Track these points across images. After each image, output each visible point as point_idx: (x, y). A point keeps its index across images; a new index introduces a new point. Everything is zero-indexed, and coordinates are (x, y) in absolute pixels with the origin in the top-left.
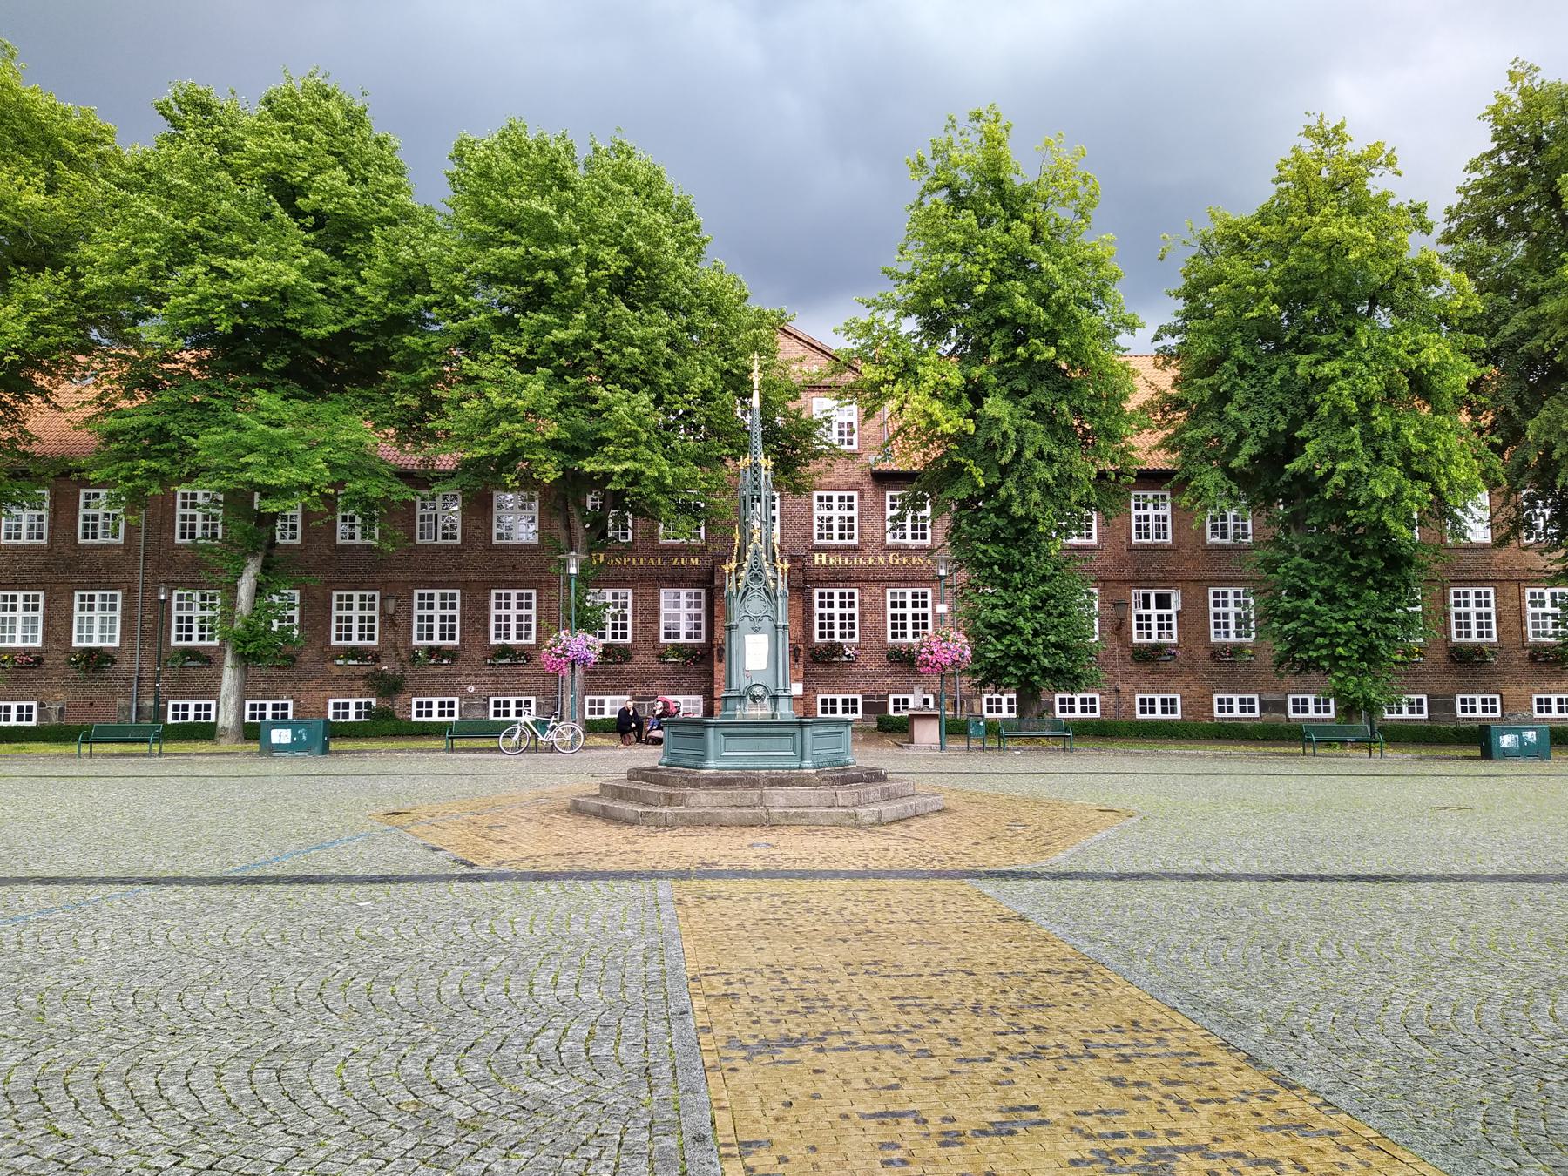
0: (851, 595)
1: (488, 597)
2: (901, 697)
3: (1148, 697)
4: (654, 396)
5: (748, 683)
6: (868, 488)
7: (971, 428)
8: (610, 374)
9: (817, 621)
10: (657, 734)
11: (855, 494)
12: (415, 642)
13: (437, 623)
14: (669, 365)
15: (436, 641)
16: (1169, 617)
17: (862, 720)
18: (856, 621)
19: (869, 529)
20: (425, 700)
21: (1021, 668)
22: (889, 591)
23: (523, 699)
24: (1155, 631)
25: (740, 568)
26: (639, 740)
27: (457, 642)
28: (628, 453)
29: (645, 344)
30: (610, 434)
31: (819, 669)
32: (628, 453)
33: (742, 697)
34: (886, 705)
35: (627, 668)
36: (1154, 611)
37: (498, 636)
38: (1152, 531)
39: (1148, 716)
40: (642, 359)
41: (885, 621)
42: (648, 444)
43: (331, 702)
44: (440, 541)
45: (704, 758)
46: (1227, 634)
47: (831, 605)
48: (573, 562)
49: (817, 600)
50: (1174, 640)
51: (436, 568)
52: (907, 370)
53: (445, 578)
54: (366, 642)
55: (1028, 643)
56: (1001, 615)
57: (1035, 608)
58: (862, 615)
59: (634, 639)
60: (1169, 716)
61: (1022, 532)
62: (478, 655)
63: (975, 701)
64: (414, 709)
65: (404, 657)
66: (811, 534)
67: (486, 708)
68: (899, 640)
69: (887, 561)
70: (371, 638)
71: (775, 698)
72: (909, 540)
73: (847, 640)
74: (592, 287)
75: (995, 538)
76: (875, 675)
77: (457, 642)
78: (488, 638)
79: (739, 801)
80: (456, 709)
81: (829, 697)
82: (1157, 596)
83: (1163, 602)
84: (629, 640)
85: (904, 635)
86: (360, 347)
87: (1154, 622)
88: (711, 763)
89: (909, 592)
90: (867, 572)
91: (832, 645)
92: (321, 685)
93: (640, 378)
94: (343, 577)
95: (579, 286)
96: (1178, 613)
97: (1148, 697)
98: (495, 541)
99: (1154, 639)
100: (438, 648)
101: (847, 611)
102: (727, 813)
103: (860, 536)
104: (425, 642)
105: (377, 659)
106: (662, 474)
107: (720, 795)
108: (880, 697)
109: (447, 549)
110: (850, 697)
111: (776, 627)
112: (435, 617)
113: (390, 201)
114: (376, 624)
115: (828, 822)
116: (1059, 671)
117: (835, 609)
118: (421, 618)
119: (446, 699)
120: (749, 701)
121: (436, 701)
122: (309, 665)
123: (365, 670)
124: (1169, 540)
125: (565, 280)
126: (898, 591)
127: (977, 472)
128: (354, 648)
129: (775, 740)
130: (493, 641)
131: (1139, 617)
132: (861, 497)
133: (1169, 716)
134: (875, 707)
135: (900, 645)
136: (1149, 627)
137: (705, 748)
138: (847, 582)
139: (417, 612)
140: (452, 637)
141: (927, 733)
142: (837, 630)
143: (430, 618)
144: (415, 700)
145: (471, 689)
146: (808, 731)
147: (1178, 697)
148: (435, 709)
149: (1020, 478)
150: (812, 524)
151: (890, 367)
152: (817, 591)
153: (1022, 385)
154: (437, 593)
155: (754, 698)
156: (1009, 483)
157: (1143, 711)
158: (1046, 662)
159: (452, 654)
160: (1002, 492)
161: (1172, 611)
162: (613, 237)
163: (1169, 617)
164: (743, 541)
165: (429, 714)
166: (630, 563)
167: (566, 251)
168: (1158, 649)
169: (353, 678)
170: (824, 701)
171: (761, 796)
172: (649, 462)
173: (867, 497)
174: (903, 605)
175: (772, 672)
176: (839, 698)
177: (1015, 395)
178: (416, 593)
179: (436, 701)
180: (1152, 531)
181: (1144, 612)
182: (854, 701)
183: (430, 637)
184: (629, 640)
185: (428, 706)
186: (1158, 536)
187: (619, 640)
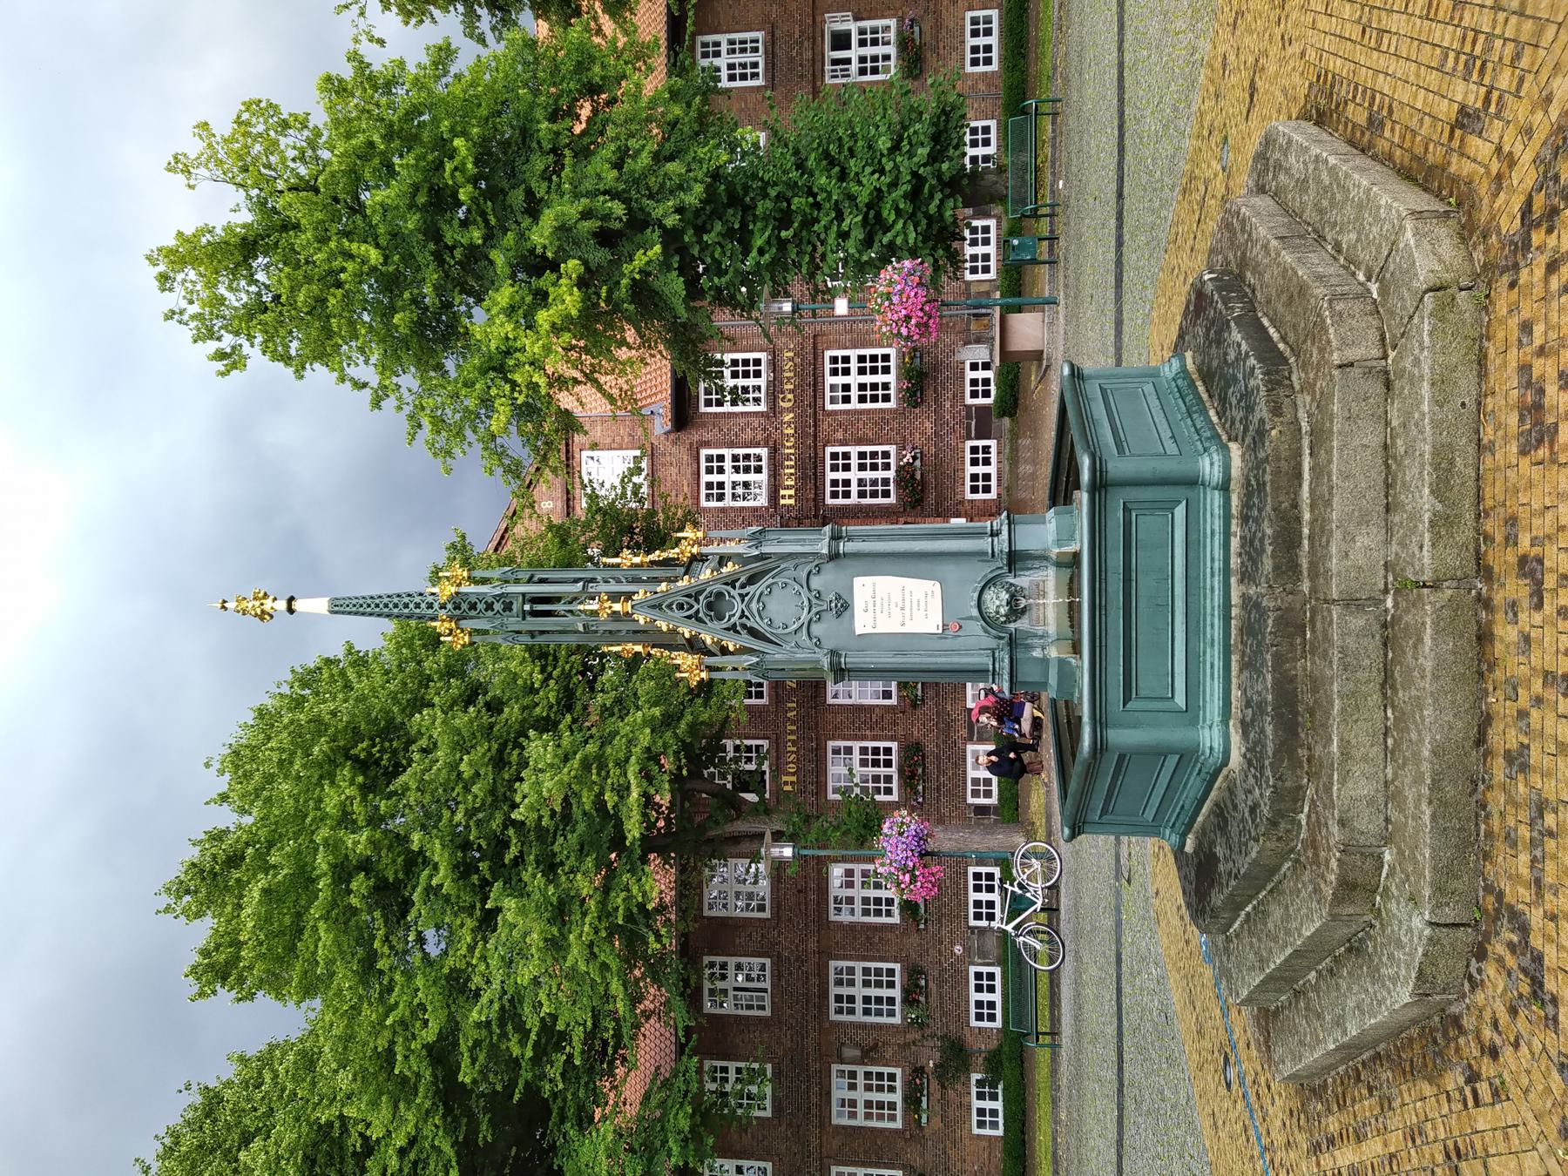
0: (834, 456)
1: (840, 925)
2: (968, 389)
3: (969, 56)
4: (532, 733)
5: (976, 627)
6: (695, 436)
7: (572, 266)
8: (502, 797)
9: (868, 501)
10: (1026, 726)
11: (704, 452)
12: (897, 1020)
13: (873, 992)
14: (495, 707)
15: (896, 993)
16: (862, 32)
17: (999, 439)
18: (868, 449)
19: (748, 435)
20: (973, 1010)
21: (931, 197)
22: (829, 407)
23: (971, 882)
24: (880, 50)
25: (693, 645)
26: (1033, 748)
27: (897, 967)
28: (615, 772)
29: (462, 746)
30: (587, 800)
31: (931, 497)
32: (615, 772)
33: (1013, 643)
34: (979, 408)
35: (930, 748)
36: (854, 53)
37: (889, 913)
38: (748, 58)
39: (995, 54)
40: (480, 750)
41: (868, 411)
42: (606, 741)
43: (976, 1131)
44: (767, 985)
45: (1187, 755)
46: (887, 58)
47: (847, 483)
48: (775, 851)
49: (841, 501)
50: (892, 23)
51: (802, 991)
52: (499, 365)
53: (814, 980)
54: (898, 1084)
55: (894, 185)
56: (852, 220)
57: (843, 176)
58: (859, 442)
59: (892, 739)
60: (995, 26)
61: (729, 198)
62: (914, 939)
63: (974, 289)
64: (985, 1024)
65: (918, 1036)
66: (755, 509)
67: (982, 931)
68: (892, 392)
69: (789, 410)
70: (892, 1077)
71: (1015, 560)
72: (762, 382)
73: (892, 461)
74: (375, 820)
75: (743, 238)
76: (939, 421)
77: (897, 967)
78: (892, 926)
79: (1369, 676)
80: (985, 970)
81: (968, 484)
82: (834, 49)
83: (841, 41)
84: (894, 745)
85: (886, 386)
86: (485, 1133)
87: (869, 51)
88: (1209, 738)
89: (830, 380)
90: (804, 435)
91: (900, 481)
92: (954, 1143)
93: (506, 761)
94: (814, 1111)
95: (372, 842)
96: (856, 19)
97: (969, 56)
98: (767, 914)
99: (891, 50)
100: (906, 992)
101: (854, 462)
102: (1433, 724)
103: (757, 445)
104: (897, 1007)
105: (919, 1071)
106: (648, 722)
107: (1347, 733)
108: (969, 417)
109: (777, 976)
110: (968, 456)
111: (834, 556)
112: (865, 992)
113: (290, 1086)
114: (875, 1069)
115: (1466, 382)
116: (935, 138)
117: (854, 474)
118: (867, 1012)
119: (972, 982)
120: (1022, 624)
121: (975, 996)
122: (928, 1156)
123: (935, 1084)
124: (760, 35)
125: (365, 866)
126: (828, 394)
127: (640, 260)
128: (905, 1099)
129: (1141, 559)
130: (896, 919)
131: (863, 72)
132: (707, 444)
133: (995, 26)
134: (983, 423)
135: (899, 390)
136: (875, 59)
137: (1158, 753)
138: (817, 462)
139: (859, 1017)
140: (891, 972)
141: (1028, 330)
142: (880, 474)
143: (867, 1000)
144: (974, 1023)
145: (958, 949)
146: (1117, 467)
147: (969, 14)
148: (985, 997)
149: (651, 197)
150: (742, 509)
151: (493, 392)
152: (829, 501)
153: (517, 197)
154: (834, 991)
155: (1015, 612)
156: (658, 212)
157: (988, 61)
158: (923, 152)
159: (914, 974)
160: (671, 221)
161: (853, 27)
162: (310, 789)
163: (862, 32)
164: (638, 634)
165: (991, 1005)
166: (794, 743)
167: (322, 862)
168: (904, 43)
169: (945, 1103)
170: (974, 490)
171: (1351, 603)
172: (631, 742)
173: (707, 437)
174: (846, 387)
175: (950, 569)
176: (970, 470)
177: (534, 208)
178: (834, 1017)
179: (975, 996)
180: (748, 58)
181: (854, 66)
182: (974, 450)
183: (891, 1001)
184: (894, 745)
185: (984, 1003)
186: (755, 50)
187: (894, 757)
